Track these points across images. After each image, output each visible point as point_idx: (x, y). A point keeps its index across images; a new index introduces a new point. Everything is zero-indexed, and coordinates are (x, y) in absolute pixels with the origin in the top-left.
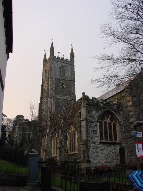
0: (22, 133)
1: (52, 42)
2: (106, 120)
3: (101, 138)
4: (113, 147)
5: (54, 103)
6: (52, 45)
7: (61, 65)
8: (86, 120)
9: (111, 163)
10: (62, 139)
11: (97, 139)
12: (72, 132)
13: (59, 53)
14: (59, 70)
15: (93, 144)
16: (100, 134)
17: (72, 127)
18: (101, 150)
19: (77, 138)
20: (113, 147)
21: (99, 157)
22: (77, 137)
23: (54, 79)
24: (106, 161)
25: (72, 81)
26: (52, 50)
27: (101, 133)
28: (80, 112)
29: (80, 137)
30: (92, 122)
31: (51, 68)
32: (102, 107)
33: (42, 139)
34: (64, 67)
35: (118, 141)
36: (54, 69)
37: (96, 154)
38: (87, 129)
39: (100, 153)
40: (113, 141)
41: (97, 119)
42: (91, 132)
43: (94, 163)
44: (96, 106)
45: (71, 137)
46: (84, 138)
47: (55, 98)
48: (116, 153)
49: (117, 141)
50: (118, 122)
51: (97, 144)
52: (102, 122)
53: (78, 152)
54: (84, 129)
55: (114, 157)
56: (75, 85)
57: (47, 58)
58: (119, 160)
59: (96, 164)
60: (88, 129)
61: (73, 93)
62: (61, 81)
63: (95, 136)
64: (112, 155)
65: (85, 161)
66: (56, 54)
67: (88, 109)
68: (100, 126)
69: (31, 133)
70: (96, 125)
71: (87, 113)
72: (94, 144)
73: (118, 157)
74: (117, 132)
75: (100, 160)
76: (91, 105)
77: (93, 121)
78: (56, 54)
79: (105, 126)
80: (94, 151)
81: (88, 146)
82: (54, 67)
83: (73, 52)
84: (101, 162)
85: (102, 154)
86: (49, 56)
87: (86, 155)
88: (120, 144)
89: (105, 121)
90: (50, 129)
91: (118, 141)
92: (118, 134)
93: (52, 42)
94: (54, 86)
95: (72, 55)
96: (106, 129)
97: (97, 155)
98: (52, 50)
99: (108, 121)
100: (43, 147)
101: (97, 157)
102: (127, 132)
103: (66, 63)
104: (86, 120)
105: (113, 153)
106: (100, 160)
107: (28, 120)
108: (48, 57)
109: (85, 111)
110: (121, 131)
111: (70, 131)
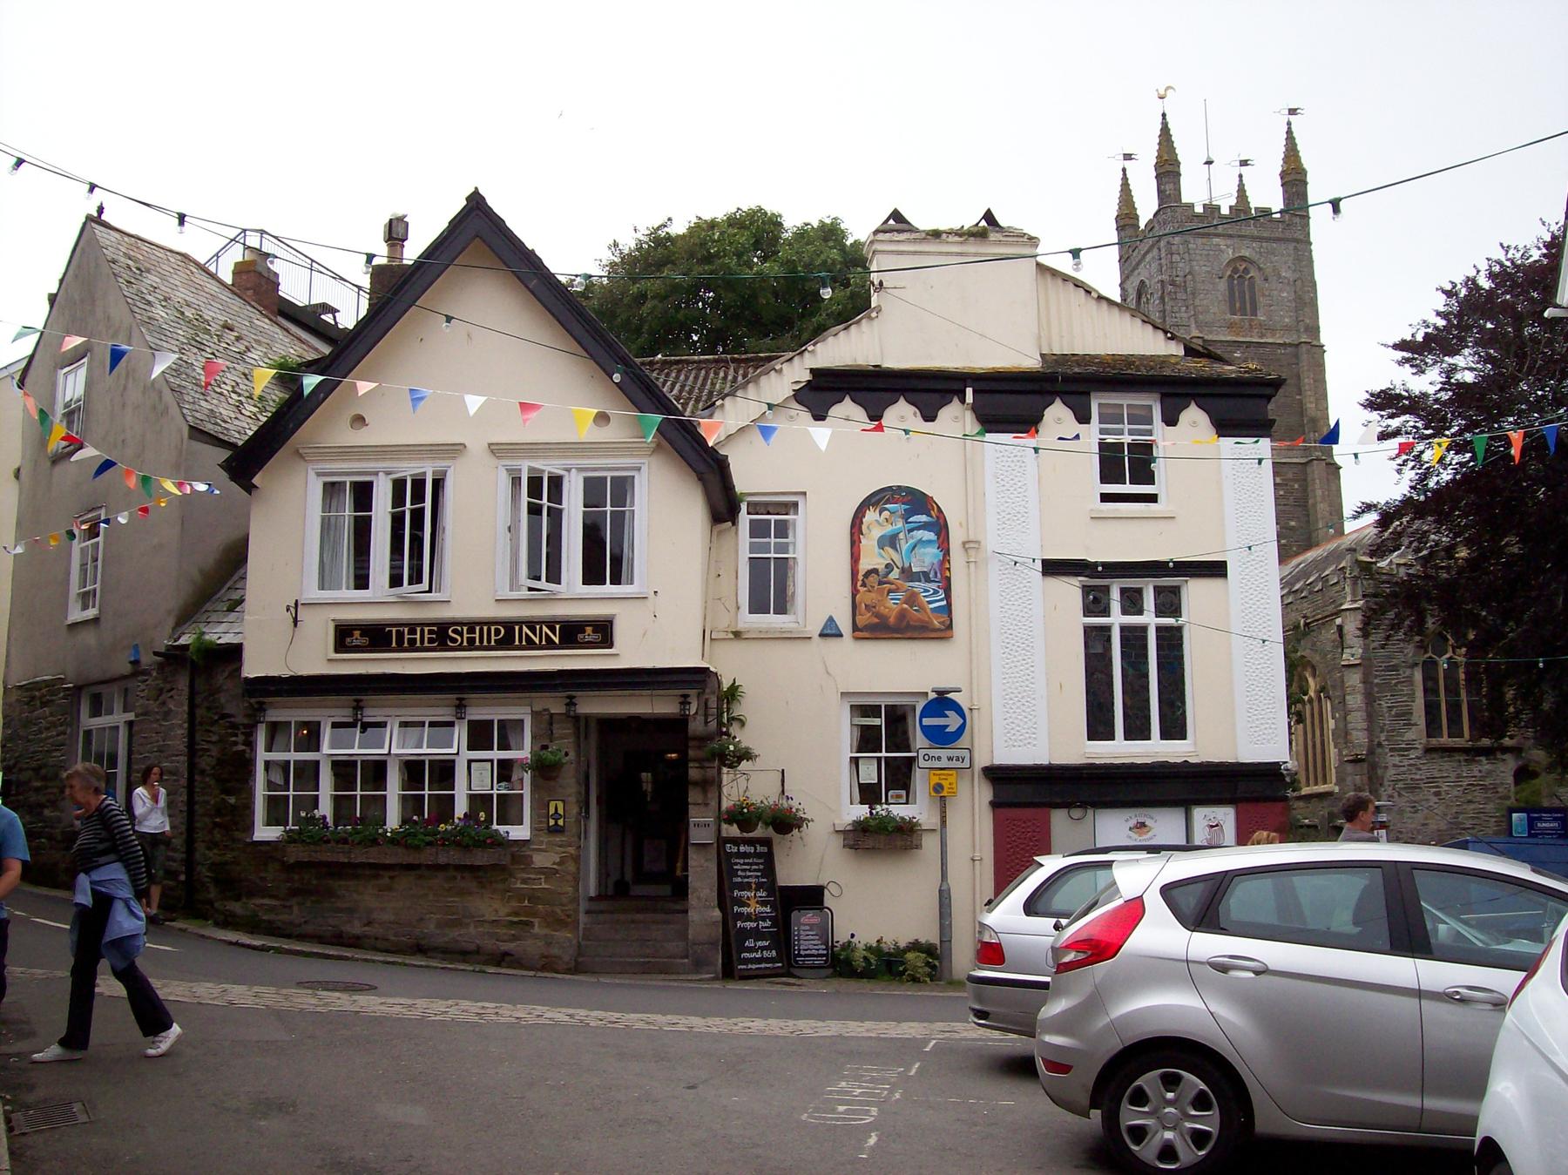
1: (1164, 115)
3: (1432, 727)
4: (1485, 765)
6: (1165, 132)
9: (1473, 828)
11: (1416, 733)
14: (1222, 285)
15: (1397, 758)
16: (1427, 713)
18: (1431, 780)
19: (1333, 730)
22: (1332, 724)
25: (1304, 348)
26: (1168, 170)
27: (1431, 709)
28: (1340, 628)
29: (1341, 725)
30: (1389, 669)
31: (1173, 283)
34: (1252, 262)
36: (1190, 285)
38: (1370, 699)
39: (1427, 794)
43: (1401, 832)
46: (1360, 737)
48: (1500, 790)
52: (1435, 663)
53: (1337, 789)
54: (1355, 701)
56: (1322, 365)
63: (1404, 725)
64: (1478, 795)
66: (1194, 192)
68: (1425, 680)
70: (1410, 681)
72: (1399, 755)
77: (1395, 662)
78: (1194, 192)
81: (1373, 767)
82: (1190, 273)
83: (1292, 133)
85: (1437, 794)
86: (1153, 205)
89: (1447, 656)
93: (1164, 115)
95: (1294, 178)
97: (1415, 802)
98: (1168, 170)
105: (1484, 788)
106: (1426, 818)
108: (1147, 206)
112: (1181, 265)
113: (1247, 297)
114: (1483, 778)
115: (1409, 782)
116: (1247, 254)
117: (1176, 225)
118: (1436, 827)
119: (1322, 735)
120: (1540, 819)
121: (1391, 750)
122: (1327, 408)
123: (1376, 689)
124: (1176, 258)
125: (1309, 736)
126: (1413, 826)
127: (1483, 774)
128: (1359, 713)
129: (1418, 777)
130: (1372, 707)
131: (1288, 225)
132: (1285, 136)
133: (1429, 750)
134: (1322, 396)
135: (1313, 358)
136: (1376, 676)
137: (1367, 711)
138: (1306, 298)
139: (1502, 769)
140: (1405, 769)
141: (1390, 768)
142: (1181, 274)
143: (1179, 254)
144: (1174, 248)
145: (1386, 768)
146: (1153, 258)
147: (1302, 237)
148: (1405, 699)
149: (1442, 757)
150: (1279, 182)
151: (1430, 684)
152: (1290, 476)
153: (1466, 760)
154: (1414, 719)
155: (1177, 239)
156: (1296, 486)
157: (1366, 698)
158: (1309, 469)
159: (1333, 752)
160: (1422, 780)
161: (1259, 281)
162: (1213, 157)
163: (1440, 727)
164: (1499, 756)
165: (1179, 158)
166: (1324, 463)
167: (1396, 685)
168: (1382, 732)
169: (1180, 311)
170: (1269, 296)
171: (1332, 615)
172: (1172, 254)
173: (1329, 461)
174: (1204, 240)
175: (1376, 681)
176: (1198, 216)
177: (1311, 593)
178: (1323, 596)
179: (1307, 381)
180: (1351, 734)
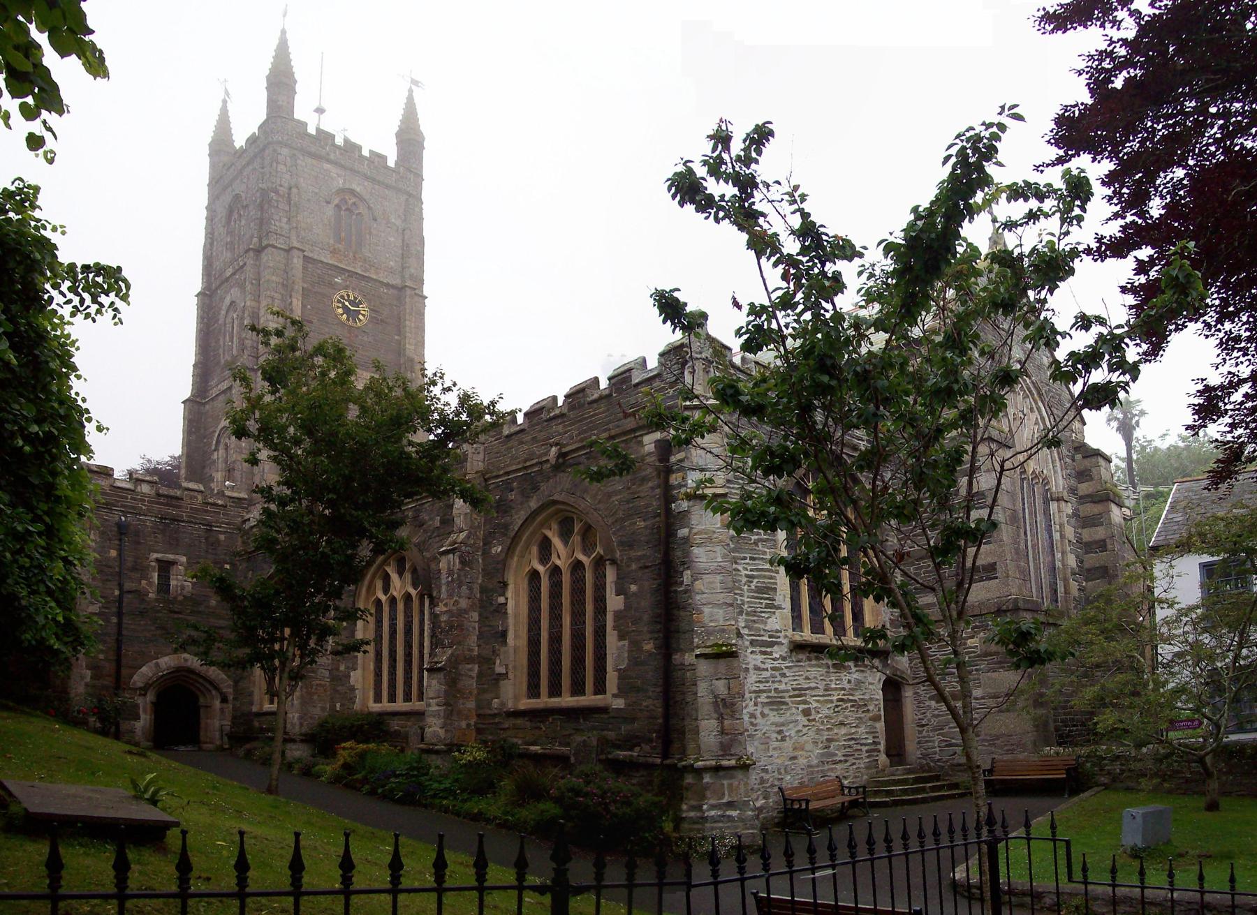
0: (113, 553)
4: (853, 674)
7: (340, 183)
8: (1156, 485)
9: (846, 761)
10: (466, 611)
14: (329, 211)
15: (760, 657)
18: (799, 692)
21: (793, 733)
24: (827, 758)
34: (361, 198)
37: (773, 717)
42: (744, 580)
48: (871, 708)
51: (777, 652)
55: (862, 730)
58: (882, 747)
59: (780, 773)
62: (338, 280)
63: (767, 606)
64: (850, 716)
65: (733, 762)
69: (174, 563)
80: (763, 698)
84: (802, 761)
85: (807, 713)
93: (283, 32)
97: (783, 725)
104: (1156, 485)
115: (773, 694)
116: (358, 190)
117: (285, 138)
121: (752, 643)
126: (779, 761)
129: (782, 687)
131: (402, 177)
134: (421, 344)
141: (752, 671)
143: (285, 165)
149: (810, 660)
153: (834, 665)
155: (285, 151)
160: (788, 691)
162: (324, 106)
167: (756, 543)
169: (280, 221)
172: (278, 163)
174: (315, 162)
180: (702, 612)
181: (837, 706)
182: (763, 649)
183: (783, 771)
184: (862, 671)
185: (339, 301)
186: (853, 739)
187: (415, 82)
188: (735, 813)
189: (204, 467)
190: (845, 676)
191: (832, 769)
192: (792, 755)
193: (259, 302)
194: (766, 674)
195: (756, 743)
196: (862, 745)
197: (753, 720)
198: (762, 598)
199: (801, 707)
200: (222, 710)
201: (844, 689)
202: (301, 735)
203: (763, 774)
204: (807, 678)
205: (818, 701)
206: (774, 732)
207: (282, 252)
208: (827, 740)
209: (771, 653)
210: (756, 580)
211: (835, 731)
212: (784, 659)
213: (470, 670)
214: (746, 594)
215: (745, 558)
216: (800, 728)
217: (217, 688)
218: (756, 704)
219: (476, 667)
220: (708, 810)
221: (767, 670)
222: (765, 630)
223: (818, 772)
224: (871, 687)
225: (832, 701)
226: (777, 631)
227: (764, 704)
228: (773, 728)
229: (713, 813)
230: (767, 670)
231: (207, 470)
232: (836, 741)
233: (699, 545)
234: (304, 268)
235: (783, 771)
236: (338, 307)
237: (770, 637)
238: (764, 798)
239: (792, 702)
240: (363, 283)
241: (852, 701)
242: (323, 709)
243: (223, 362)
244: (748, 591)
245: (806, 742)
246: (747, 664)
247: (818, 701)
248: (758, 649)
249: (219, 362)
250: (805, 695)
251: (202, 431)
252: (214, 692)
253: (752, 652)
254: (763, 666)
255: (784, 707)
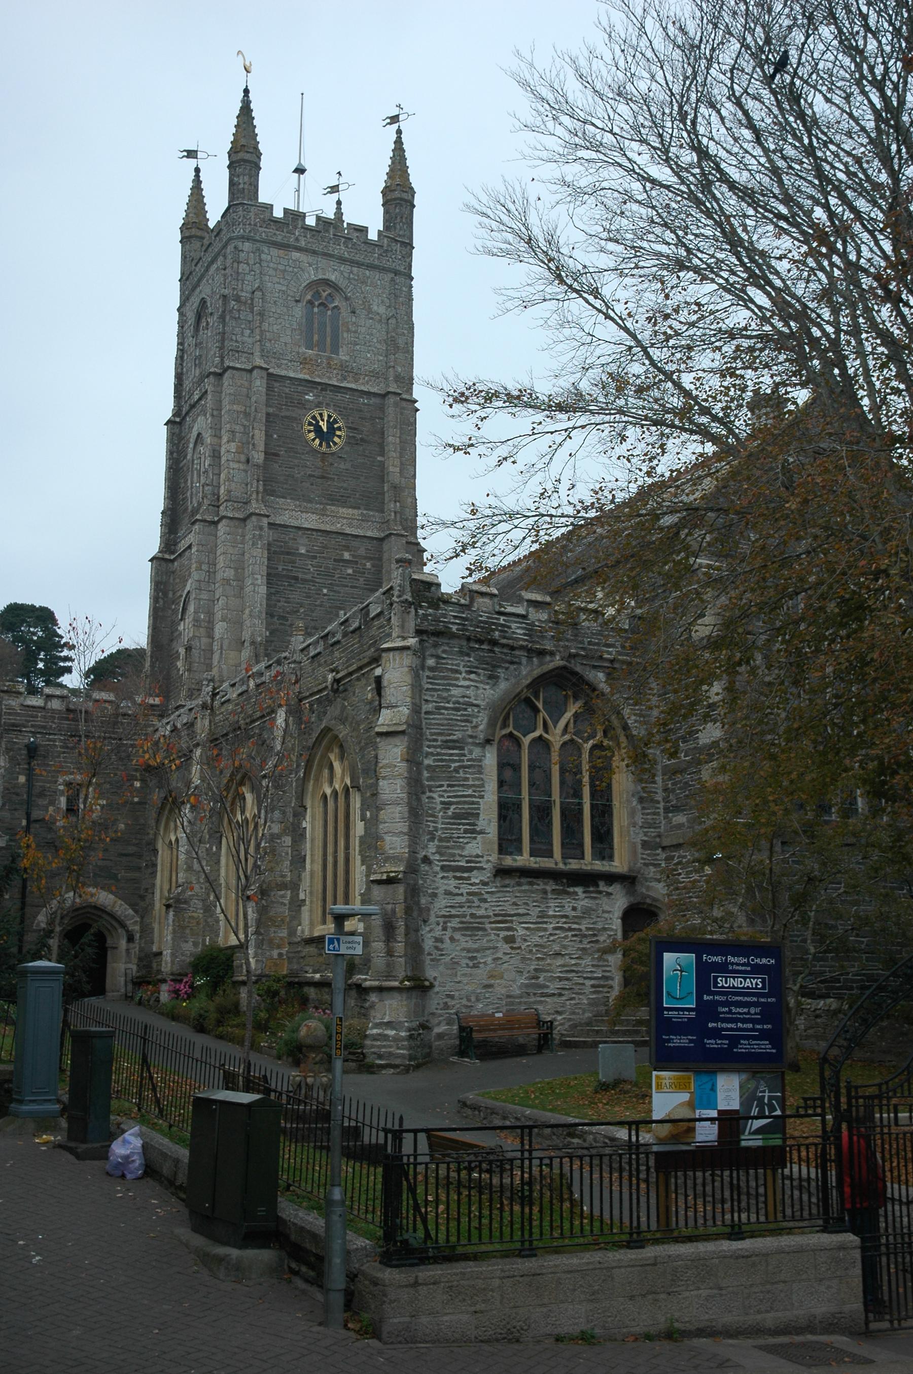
0: (22, 779)
1: (246, 91)
2: (546, 728)
4: (581, 899)
5: (257, 559)
6: (246, 112)
7: (311, 275)
9: (560, 995)
10: (279, 836)
12: (335, 793)
13: (300, 171)
14: (299, 311)
15: (453, 882)
16: (502, 817)
17: (337, 765)
18: (503, 918)
20: (586, 903)
21: (489, 960)
23: (259, 383)
24: (534, 987)
25: (391, 400)
28: (378, 680)
31: (238, 299)
32: (522, 648)
33: (158, 821)
35: (618, 864)
36: (258, 302)
37: (465, 942)
39: (494, 937)
40: (589, 863)
41: (482, 721)
42: (439, 807)
43: (452, 997)
44: (481, 642)
45: (330, 828)
47: (265, 521)
48: (602, 939)
49: (611, 858)
50: (623, 739)
51: (476, 877)
52: (518, 743)
55: (587, 961)
57: (214, 215)
60: (422, 786)
61: (395, 487)
62: (310, 397)
63: (466, 831)
64: (572, 948)
67: (431, 662)
68: (501, 766)
71: (416, 687)
72: (456, 878)
73: (615, 960)
74: (616, 803)
75: (491, 977)
76: (453, 636)
77: (458, 735)
79: (539, 769)
81: (414, 892)
82: (259, 289)
84: (500, 991)
85: (510, 940)
87: (399, 947)
88: (628, 880)
89: (536, 734)
90: (210, 762)
91: (616, 863)
92: (620, 820)
93: (246, 91)
94: (259, 436)
96: (541, 784)
97: (477, 951)
99: (556, 738)
100: (167, 874)
101: (472, 958)
102: (677, 809)
103: (353, 263)
107: (363, 230)
109: (408, 679)
110: (641, 800)
111: (328, 791)
112: (248, 277)
113: (328, 329)
114: (578, 919)
116: (333, 278)
117: (248, 228)
118: (503, 991)
119: (347, 847)
120: (723, 968)
121: (443, 868)
122: (414, 476)
123: (426, 774)
124: (243, 267)
125: (330, 850)
126: (469, 988)
127: (578, 914)
128: (399, 809)
129: (482, 912)
130: (419, 800)
132: (393, 146)
133: (502, 872)
135: (402, 414)
136: (428, 754)
137: (409, 804)
138: (401, 342)
139: (607, 908)
140: (463, 899)
141: (441, 897)
142: (249, 288)
143: (248, 264)
144: (242, 255)
145: (435, 895)
146: (218, 269)
147: (402, 269)
148: (470, 792)
149: (519, 884)
150: (380, 200)
151: (508, 774)
152: (362, 552)
154: (481, 824)
155: (247, 246)
156: (368, 565)
157: (409, 784)
158: (386, 546)
159: (359, 871)
160: (488, 917)
161: (345, 313)
163: (519, 840)
164: (602, 886)
165: (261, 147)
166: (404, 540)
167: (456, 770)
168: (432, 839)
170: (356, 332)
171: (369, 664)
173: (412, 540)
175: (427, 762)
176: (276, 221)
177: (345, 635)
178: (361, 636)
179: (392, 439)
180: (383, 840)
181: (551, 935)
182: (458, 874)
183: (473, 999)
184: (595, 898)
185: (310, 424)
186: (573, 971)
187: (191, 154)
188: (392, 1033)
189: (172, 640)
190: (568, 904)
191: (541, 1002)
192: (486, 982)
193: (220, 438)
194: (459, 899)
195: (441, 968)
196: (585, 978)
197: (439, 944)
198: (459, 824)
199: (503, 934)
200: (128, 950)
201: (566, 916)
202: (172, 974)
203: (448, 1000)
204: (515, 904)
205: (527, 929)
206: (465, 957)
207: (244, 373)
208: (536, 970)
209: (469, 878)
210: (453, 807)
211: (549, 961)
212: (485, 884)
213: (283, 896)
214: (440, 821)
215: (442, 786)
216: (500, 955)
217: (123, 926)
218: (445, 929)
219: (289, 892)
220: (372, 1028)
221: (462, 895)
222: (461, 856)
223: (520, 1003)
224: (606, 915)
225: (545, 930)
226: (478, 856)
227: (455, 929)
228: (464, 954)
229: (375, 1031)
230: (462, 895)
231: (175, 643)
232: (548, 971)
233: (384, 778)
234: (269, 388)
235: (473, 999)
236: (310, 431)
237: (468, 862)
238: (448, 1024)
239: (492, 929)
240: (339, 396)
241: (574, 929)
242: (195, 944)
243: (190, 508)
244: (443, 817)
245: (506, 970)
246: (437, 888)
247: (527, 929)
248: (450, 874)
249: (187, 509)
250: (512, 922)
251: (170, 595)
252: (120, 930)
253: (443, 878)
254: (457, 891)
255: (480, 933)
